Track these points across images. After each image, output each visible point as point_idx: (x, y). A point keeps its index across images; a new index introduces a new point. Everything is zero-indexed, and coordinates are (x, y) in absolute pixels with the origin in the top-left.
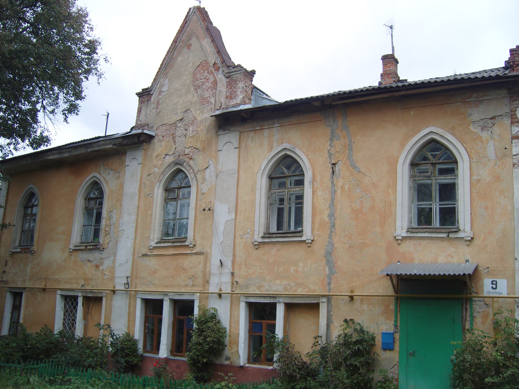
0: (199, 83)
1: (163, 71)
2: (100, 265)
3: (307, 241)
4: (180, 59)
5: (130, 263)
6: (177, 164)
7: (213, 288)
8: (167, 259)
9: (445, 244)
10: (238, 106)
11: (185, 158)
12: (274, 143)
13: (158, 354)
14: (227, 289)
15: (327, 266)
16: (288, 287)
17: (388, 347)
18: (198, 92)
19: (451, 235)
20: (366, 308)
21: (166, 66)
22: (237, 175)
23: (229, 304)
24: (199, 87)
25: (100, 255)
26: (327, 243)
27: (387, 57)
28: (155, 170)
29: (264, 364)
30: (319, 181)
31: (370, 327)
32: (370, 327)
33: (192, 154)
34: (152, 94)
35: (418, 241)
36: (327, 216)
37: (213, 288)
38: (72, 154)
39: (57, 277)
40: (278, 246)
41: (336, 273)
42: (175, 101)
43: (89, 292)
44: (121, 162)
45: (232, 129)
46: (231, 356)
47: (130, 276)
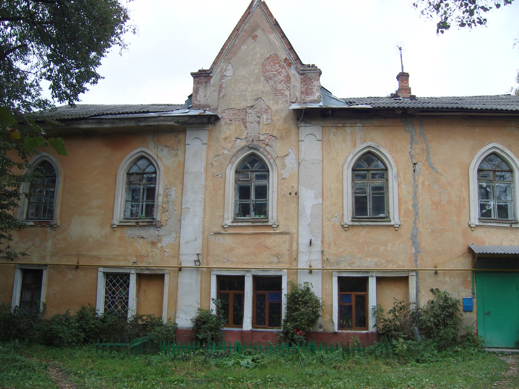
0: (270, 75)
1: (224, 56)
2: (157, 243)
3: (395, 226)
4: (244, 47)
5: (200, 241)
6: (251, 148)
7: (303, 264)
8: (246, 237)
9: (508, 232)
10: (316, 102)
11: (261, 143)
12: (357, 141)
13: (242, 327)
14: (317, 265)
15: (413, 247)
16: (379, 264)
17: (468, 309)
18: (269, 82)
19: (513, 226)
20: (448, 280)
21: (227, 51)
22: (321, 164)
23: (321, 279)
24: (270, 78)
25: (157, 232)
26: (412, 228)
27: (404, 75)
28: (224, 151)
29: (355, 330)
30: (402, 177)
31: (453, 294)
32: (453, 294)
33: (268, 140)
34: (212, 77)
35: (488, 229)
36: (411, 205)
37: (303, 264)
38: (116, 126)
39: (95, 253)
40: (367, 229)
41: (421, 252)
42: (242, 87)
43: (145, 269)
44: (177, 139)
45: (313, 122)
46: (324, 324)
47: (200, 253)
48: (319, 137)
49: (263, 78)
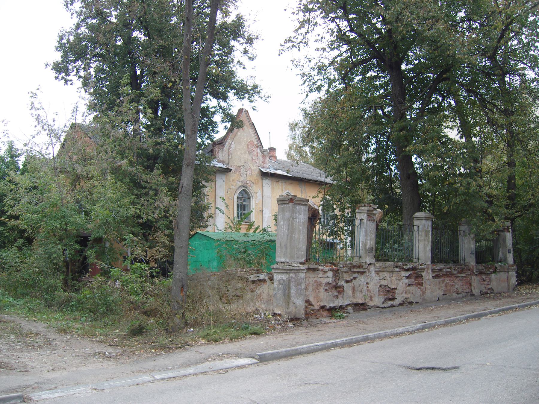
48: (270, 186)
49: (247, 152)
